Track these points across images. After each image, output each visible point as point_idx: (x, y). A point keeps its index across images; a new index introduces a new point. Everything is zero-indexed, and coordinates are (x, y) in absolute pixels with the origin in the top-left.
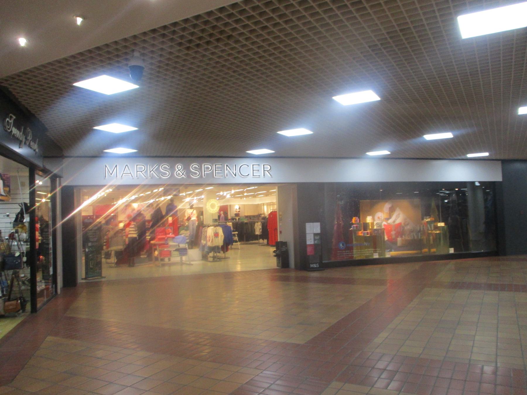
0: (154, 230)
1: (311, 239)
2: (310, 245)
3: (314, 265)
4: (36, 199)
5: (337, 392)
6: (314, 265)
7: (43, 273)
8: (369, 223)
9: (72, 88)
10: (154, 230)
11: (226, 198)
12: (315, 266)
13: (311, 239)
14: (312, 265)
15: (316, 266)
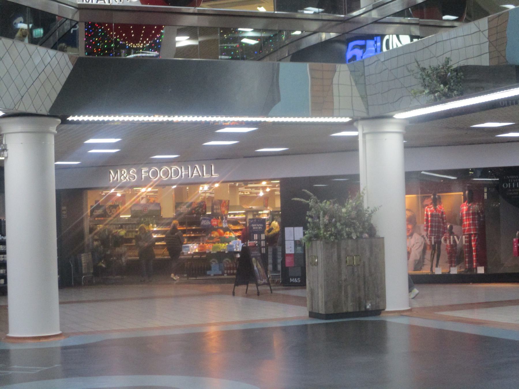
0: (96, 203)
1: (291, 247)
2: (290, 255)
3: (294, 280)
4: (138, 258)
5: (21, 76)
6: (294, 280)
7: (456, 249)
8: (442, 272)
9: (118, 233)
10: (96, 203)
11: (116, 197)
12: (295, 280)
13: (291, 247)
14: (292, 279)
15: (296, 281)
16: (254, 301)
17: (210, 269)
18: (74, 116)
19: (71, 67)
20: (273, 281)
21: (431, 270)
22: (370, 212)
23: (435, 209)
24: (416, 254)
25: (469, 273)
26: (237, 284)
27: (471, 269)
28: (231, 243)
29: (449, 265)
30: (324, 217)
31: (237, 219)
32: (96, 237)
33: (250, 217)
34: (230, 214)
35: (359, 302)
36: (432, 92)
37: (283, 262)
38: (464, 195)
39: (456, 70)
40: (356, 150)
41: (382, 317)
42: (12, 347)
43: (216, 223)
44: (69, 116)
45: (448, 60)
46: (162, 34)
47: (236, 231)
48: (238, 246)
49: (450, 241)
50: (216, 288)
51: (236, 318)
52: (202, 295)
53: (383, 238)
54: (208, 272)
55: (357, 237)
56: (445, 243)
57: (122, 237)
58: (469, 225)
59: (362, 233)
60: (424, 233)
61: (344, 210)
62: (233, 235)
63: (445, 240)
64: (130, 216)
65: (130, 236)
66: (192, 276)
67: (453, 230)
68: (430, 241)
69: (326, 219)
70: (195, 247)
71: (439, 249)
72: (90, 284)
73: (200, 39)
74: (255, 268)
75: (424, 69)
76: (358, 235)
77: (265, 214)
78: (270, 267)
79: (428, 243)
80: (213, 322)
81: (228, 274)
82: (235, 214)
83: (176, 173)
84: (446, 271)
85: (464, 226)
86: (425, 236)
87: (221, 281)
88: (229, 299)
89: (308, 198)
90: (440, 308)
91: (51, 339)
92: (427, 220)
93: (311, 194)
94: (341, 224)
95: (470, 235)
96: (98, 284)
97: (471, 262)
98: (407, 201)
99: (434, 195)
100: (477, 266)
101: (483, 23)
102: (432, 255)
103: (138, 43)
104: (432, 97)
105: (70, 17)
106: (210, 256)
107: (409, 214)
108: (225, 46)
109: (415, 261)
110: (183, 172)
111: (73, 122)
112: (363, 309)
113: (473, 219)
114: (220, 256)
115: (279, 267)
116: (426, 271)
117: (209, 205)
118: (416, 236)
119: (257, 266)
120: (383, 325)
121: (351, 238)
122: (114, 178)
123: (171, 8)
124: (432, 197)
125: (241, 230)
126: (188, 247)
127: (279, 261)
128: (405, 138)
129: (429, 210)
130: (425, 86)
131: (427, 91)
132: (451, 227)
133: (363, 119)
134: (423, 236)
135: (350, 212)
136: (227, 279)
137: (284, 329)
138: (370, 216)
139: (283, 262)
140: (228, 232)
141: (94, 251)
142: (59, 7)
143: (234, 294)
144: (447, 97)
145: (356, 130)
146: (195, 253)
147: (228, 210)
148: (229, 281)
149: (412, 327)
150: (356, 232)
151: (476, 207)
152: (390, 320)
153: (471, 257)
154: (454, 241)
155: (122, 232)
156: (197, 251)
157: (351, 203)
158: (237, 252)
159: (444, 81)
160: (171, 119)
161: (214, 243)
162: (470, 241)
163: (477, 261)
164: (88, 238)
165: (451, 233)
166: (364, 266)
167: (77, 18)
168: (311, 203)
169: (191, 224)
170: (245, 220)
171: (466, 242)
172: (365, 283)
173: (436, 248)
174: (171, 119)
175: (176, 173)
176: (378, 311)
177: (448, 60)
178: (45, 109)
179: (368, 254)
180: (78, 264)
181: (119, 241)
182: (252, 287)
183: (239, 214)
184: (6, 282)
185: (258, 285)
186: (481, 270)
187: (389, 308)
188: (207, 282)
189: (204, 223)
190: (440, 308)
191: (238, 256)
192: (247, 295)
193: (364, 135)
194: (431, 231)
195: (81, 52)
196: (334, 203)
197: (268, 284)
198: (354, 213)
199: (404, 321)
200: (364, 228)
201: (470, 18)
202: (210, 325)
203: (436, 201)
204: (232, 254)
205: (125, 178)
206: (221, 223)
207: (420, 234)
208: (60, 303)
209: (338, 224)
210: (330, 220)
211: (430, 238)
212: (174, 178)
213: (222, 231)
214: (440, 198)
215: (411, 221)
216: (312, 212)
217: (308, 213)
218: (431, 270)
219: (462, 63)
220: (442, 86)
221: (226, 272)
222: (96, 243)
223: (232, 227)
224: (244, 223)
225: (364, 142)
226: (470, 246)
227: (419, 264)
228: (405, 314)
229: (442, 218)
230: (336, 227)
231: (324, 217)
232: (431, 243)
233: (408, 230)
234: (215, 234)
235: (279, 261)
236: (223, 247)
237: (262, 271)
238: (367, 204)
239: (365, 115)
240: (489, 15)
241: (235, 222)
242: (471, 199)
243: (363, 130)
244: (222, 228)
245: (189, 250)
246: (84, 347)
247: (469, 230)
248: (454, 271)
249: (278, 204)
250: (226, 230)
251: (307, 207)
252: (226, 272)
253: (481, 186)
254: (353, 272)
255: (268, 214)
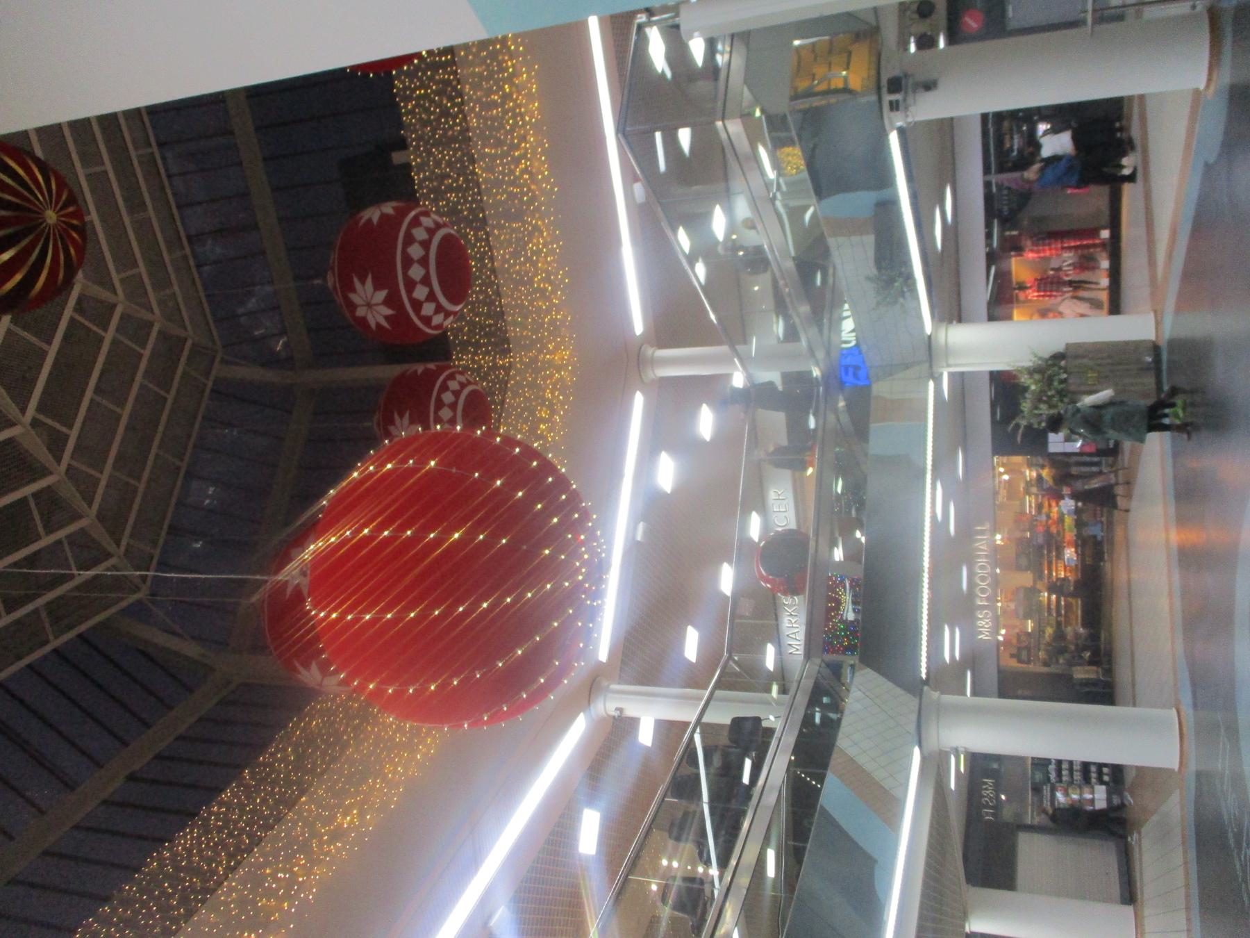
16: (1137, 491)
17: (1095, 537)
18: (921, 672)
19: (868, 670)
20: (1112, 466)
21: (1103, 289)
22: (1036, 359)
23: (1030, 287)
24: (1083, 308)
25: (1109, 248)
26: (1115, 506)
27: (1103, 245)
28: (1065, 512)
29: (1097, 271)
30: (1040, 409)
31: (1036, 506)
32: (1054, 660)
33: (1034, 490)
34: (1030, 512)
35: (1145, 369)
36: (902, 294)
37: (1090, 455)
38: (1015, 256)
39: (879, 268)
40: (962, 374)
41: (1163, 344)
42: (1192, 767)
43: (1041, 528)
44: (921, 678)
45: (868, 278)
46: (832, 575)
47: (1050, 506)
48: (1068, 504)
49: (1070, 270)
50: (1119, 533)
51: (1159, 510)
52: (1128, 548)
53: (1067, 344)
54: (1099, 538)
55: (1065, 372)
56: (1072, 275)
57: (1055, 632)
58: (1050, 249)
59: (1060, 368)
60: (1059, 299)
61: (1033, 387)
62: (1055, 509)
63: (1067, 275)
64: (1030, 621)
65: (1054, 623)
66: (1104, 557)
67: (1057, 266)
68: (1069, 292)
69: (1043, 407)
70: (1069, 551)
71: (1075, 282)
72: (1109, 671)
73: (837, 535)
74: (1097, 486)
75: (878, 304)
76: (1062, 371)
77: (1030, 474)
78: (1094, 469)
79: (1070, 294)
80: (1163, 535)
81: (1102, 516)
82: (1030, 506)
83: (982, 568)
84: (1105, 274)
85: (1051, 255)
86: (1063, 297)
87: (1110, 525)
88: (1133, 515)
89: (1018, 426)
90: (1153, 277)
91: (1183, 720)
92: (1043, 296)
93: (1014, 422)
94: (1050, 389)
95: (1063, 248)
96: (1110, 662)
97: (1095, 246)
98: (1023, 319)
99: (1015, 289)
100: (1100, 239)
101: (832, 242)
102: (1085, 289)
103: (840, 600)
104: (908, 294)
105: (817, 668)
106: (1079, 536)
107: (1036, 317)
108: (362, 466)
109: (1091, 308)
110: (982, 561)
111: (928, 674)
112: (1152, 366)
113: (1044, 245)
114: (1079, 524)
115: (1096, 459)
116: (1104, 296)
117: (1018, 534)
118: (1061, 309)
119: (1095, 484)
120: (1174, 344)
121: (1065, 379)
122: (987, 636)
123: (617, 474)
124: (1017, 291)
125: (1049, 500)
126: (1068, 559)
127: (1088, 459)
128: (950, 322)
129: (1032, 294)
130: (896, 302)
131: (901, 300)
132: (1052, 269)
133: (931, 366)
134: (1064, 300)
135: (1035, 380)
136: (1107, 518)
137: (1176, 455)
138: (1040, 358)
139: (1090, 455)
140: (1052, 515)
141: (1070, 664)
142: (806, 677)
143: (1127, 511)
144: (909, 278)
145: (941, 374)
146: (1076, 552)
147: (1025, 513)
148: (1110, 515)
149: (1178, 310)
150: (1059, 374)
151: (1028, 243)
152: (1167, 333)
153: (1088, 247)
154: (1069, 265)
155: (1049, 631)
156: (1073, 550)
157: (1025, 379)
158: (1076, 507)
159: (890, 282)
160: (926, 570)
161: (1064, 530)
162: (1070, 248)
163: (1094, 238)
164: (1053, 669)
165: (1059, 269)
166: (1099, 365)
167: (818, 661)
168: (1023, 423)
169: (1042, 556)
170: (1037, 495)
171: (1070, 252)
172: (1120, 364)
173: (1076, 285)
174: (926, 570)
175: (982, 568)
176: (1155, 349)
177: (868, 278)
178: (913, 702)
179: (1085, 361)
180: (1086, 683)
181: (1060, 635)
182: (1119, 490)
183: (1030, 502)
184: (1105, 765)
185: (1117, 484)
186: (1105, 234)
187: (1150, 335)
188: (1111, 542)
189: (1040, 540)
190: (1153, 277)
191: (1080, 504)
192: (1129, 496)
193: (949, 366)
194: (1057, 291)
195: (851, 659)
196: (1025, 398)
197: (1116, 472)
198: (1037, 376)
199: (1168, 320)
200: (1054, 365)
201: (826, 252)
202: (1167, 540)
203: (1022, 287)
204: (1077, 511)
205: (987, 623)
206: (1041, 522)
207: (1060, 303)
208: (1134, 705)
209: (1049, 393)
210: (1045, 402)
211: (1065, 292)
212: (989, 570)
213: (1050, 522)
214: (1017, 283)
215: (1044, 314)
216: (1034, 421)
217: (1036, 426)
218: (1103, 289)
219: (871, 262)
220: (896, 284)
221: (1098, 519)
222: (1061, 661)
223: (1045, 510)
224: (1040, 497)
225: (956, 365)
226: (1076, 248)
227: (1096, 304)
228: (1159, 318)
229: (1041, 280)
230: (1053, 396)
231: (1040, 409)
232: (1069, 292)
233: (1055, 317)
234: (1054, 530)
235: (1088, 459)
236: (1069, 521)
237: (1101, 478)
238: (1027, 362)
239: (926, 365)
240: (823, 234)
241: (1039, 507)
242: (1019, 249)
243: (943, 367)
244: (1047, 521)
245: (1072, 559)
246: (1194, 684)
247: (1056, 249)
248: (1105, 264)
249: (1018, 459)
250: (1048, 517)
251: (1029, 427)
252: (1098, 519)
253: (1002, 239)
254: (1106, 377)
255: (1031, 471)
